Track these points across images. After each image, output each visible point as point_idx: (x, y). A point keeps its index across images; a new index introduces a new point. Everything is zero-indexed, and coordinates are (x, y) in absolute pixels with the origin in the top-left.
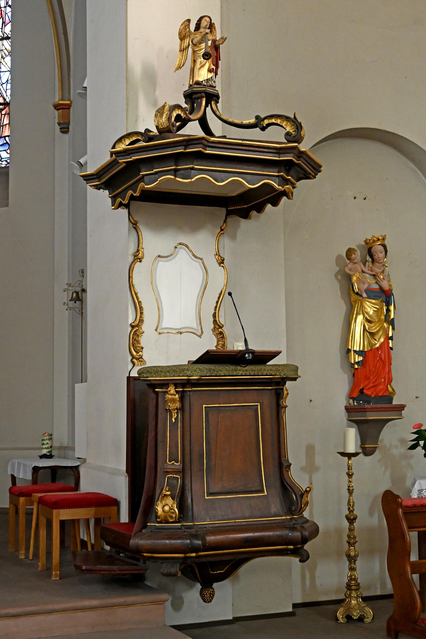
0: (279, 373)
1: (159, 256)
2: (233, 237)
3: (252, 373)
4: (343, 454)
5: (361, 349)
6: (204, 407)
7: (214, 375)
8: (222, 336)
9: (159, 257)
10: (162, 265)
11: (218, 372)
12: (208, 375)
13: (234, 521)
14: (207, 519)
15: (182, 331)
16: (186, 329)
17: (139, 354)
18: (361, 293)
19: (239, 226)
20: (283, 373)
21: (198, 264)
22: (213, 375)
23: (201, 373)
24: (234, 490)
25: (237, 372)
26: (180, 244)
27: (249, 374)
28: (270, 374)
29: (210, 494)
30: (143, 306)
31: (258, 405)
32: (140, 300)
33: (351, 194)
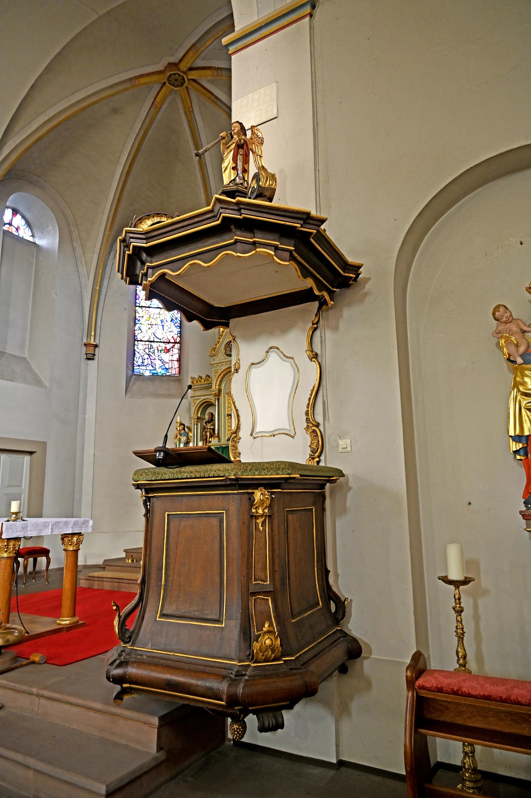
0: (228, 473)
1: (252, 364)
2: (335, 329)
3: (198, 474)
4: (445, 580)
5: (518, 432)
6: (166, 515)
7: (159, 478)
8: (315, 434)
9: (252, 364)
10: (254, 371)
11: (162, 475)
12: (153, 479)
13: (173, 654)
14: (149, 646)
15: (275, 433)
16: (278, 431)
17: (237, 460)
18: (515, 359)
19: (342, 315)
20: (233, 473)
21: (288, 364)
22: (158, 479)
23: (147, 477)
24: (188, 615)
25: (182, 474)
26: (271, 348)
27: (194, 477)
28: (217, 475)
29: (163, 615)
30: (239, 414)
31: (224, 513)
32: (238, 408)
33: (515, 240)
